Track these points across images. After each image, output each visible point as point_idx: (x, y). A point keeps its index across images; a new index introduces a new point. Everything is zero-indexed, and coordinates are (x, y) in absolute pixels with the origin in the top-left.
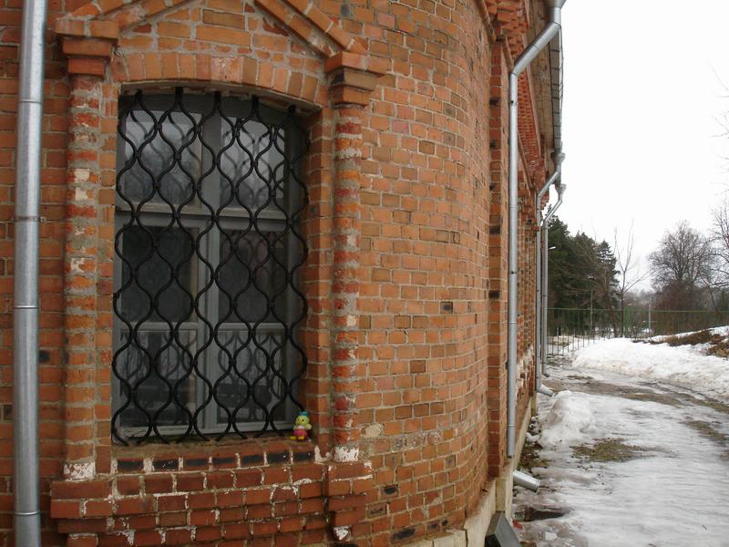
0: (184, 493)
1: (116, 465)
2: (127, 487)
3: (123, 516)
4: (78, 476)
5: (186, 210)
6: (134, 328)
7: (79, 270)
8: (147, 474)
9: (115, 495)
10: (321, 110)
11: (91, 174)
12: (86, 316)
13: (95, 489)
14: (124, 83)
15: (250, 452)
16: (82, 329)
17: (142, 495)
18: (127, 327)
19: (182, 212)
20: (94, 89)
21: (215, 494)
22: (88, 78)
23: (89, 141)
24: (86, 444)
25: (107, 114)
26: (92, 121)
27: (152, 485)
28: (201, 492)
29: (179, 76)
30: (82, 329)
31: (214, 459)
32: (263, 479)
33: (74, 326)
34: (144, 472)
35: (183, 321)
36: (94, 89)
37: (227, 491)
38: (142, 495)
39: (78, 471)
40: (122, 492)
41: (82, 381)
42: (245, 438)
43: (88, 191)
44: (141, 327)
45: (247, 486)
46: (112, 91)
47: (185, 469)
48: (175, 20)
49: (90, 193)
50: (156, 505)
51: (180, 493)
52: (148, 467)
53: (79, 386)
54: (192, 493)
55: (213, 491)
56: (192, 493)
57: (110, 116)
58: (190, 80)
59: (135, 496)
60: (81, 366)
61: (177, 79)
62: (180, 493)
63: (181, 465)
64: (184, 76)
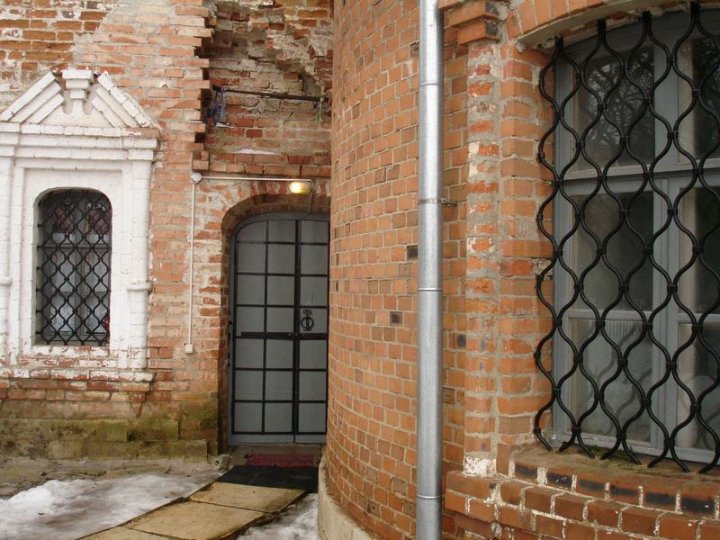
0: (561, 518)
1: (514, 468)
2: (510, 495)
3: (509, 526)
4: (470, 471)
5: (612, 171)
6: (648, 318)
7: (473, 251)
8: (540, 485)
9: (495, 498)
10: (531, 48)
11: (481, 146)
12: (477, 299)
13: (481, 487)
14: (519, 37)
15: (661, 488)
16: (474, 314)
17: (521, 507)
18: (640, 318)
19: (705, 167)
20: (482, 54)
21: (596, 530)
22: (476, 44)
23: (478, 111)
24: (477, 437)
25: (505, 77)
26: (485, 89)
27: (540, 500)
28: (579, 523)
29: (568, 11)
30: (474, 314)
31: (612, 487)
32: (657, 528)
33: (470, 309)
34: (537, 483)
35: (710, 313)
36: (482, 54)
37: (609, 530)
38: (521, 507)
39: (470, 465)
40: (505, 498)
41: (474, 369)
42: (685, 470)
43: (479, 165)
44: (608, 316)
45: (636, 532)
46: (508, 50)
47: (577, 490)
48: (114, 59)
49: (480, 168)
50: (533, 522)
51: (558, 518)
52: (542, 477)
53: (472, 374)
54: (570, 521)
55: (592, 525)
56: (570, 521)
57: (508, 79)
58: (583, 10)
59: (515, 507)
60: (473, 352)
61: (566, 15)
62: (558, 518)
63: (574, 484)
64: (574, 8)
